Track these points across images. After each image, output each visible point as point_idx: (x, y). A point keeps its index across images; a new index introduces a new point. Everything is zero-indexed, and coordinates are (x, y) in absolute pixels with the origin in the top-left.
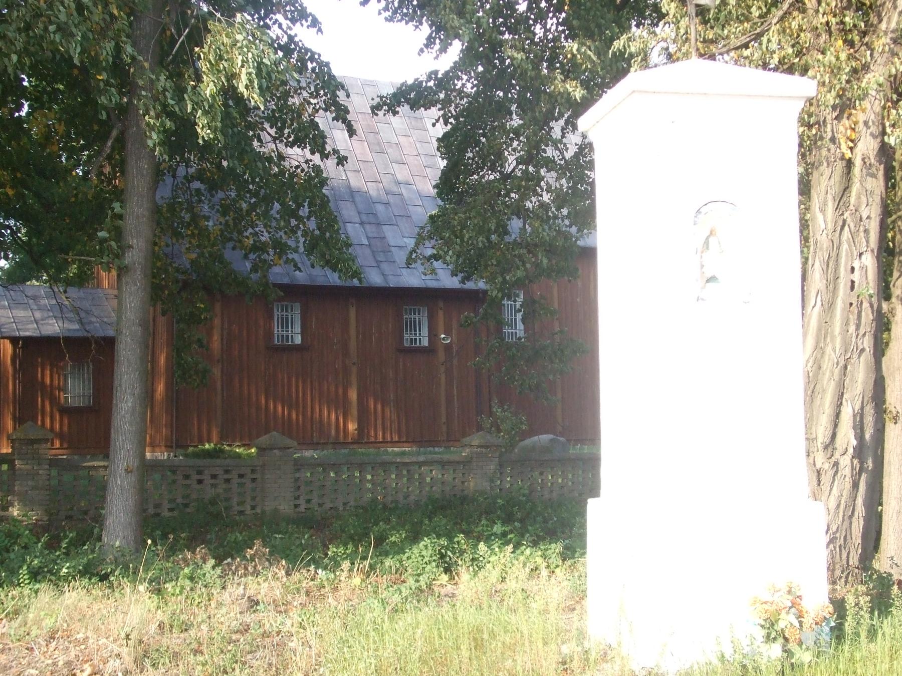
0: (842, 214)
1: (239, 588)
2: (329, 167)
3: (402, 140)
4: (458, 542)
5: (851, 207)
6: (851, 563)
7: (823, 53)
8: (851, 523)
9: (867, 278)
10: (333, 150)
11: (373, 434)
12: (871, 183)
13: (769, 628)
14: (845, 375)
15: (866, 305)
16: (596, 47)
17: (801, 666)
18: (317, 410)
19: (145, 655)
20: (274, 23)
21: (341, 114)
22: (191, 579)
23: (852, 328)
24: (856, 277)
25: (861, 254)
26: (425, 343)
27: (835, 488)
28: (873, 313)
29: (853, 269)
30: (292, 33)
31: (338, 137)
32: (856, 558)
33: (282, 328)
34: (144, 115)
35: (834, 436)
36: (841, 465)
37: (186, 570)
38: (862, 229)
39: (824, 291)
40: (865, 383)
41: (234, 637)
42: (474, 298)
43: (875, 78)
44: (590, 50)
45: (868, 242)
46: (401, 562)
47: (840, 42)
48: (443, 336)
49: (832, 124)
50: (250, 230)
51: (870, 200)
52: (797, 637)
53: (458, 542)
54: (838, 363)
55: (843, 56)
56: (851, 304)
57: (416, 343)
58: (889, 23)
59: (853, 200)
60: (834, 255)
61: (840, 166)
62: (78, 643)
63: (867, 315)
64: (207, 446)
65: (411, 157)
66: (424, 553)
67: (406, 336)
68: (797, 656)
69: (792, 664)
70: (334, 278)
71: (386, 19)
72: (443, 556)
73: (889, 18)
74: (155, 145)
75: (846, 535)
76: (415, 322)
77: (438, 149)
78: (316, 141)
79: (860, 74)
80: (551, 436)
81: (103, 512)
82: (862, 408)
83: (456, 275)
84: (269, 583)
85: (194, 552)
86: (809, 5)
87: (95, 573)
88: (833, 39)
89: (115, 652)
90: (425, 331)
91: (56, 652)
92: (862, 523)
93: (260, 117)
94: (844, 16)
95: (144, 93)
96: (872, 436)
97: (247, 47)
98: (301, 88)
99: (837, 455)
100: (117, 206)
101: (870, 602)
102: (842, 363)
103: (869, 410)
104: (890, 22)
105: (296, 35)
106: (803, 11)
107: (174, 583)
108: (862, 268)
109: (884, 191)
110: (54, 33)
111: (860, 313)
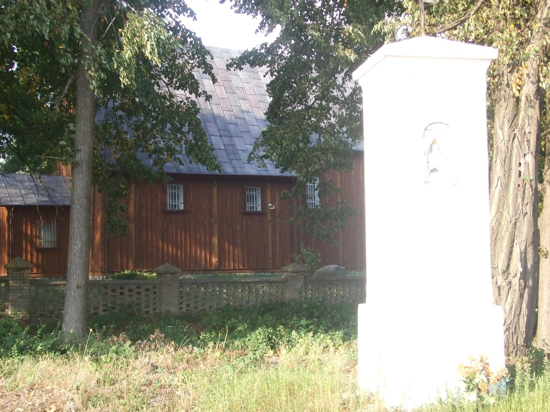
0: (514, 131)
1: (146, 358)
2: (201, 102)
3: (245, 85)
4: (279, 331)
5: (519, 126)
6: (519, 343)
7: (502, 32)
8: (519, 319)
9: (528, 169)
10: (203, 91)
11: (227, 264)
12: (531, 112)
13: (469, 383)
14: (515, 228)
15: (528, 186)
16: (363, 29)
17: (488, 406)
18: (193, 250)
19: (89, 399)
20: (167, 14)
21: (208, 70)
22: (117, 353)
23: (520, 200)
24: (522, 169)
25: (525, 155)
26: (259, 209)
27: (509, 298)
28: (532, 191)
29: (520, 164)
30: (178, 20)
31: (206, 84)
32: (522, 340)
33: (172, 200)
34: (88, 70)
35: (508, 266)
36: (513, 284)
37: (114, 348)
38: (525, 139)
39: (503, 177)
40: (528, 233)
41: (143, 388)
42: (289, 182)
43: (533, 47)
44: (360, 31)
45: (529, 147)
46: (244, 342)
47: (512, 26)
48: (270, 205)
49: (507, 76)
50: (153, 140)
51: (531, 122)
52: (486, 388)
53: (279, 331)
54: (511, 221)
55: (514, 34)
56: (519, 185)
57: (253, 209)
58: (542, 14)
59: (520, 122)
60: (508, 155)
61: (512, 101)
62: (48, 392)
63: (529, 192)
64: (126, 272)
65: (251, 96)
66: (259, 337)
67: (247, 205)
68: (486, 400)
69: (483, 405)
70: (203, 170)
71: (235, 12)
72: (270, 339)
73: (542, 11)
74: (94, 88)
75: (516, 326)
76: (253, 196)
77: (267, 91)
78: (193, 86)
79: (525, 45)
80: (336, 266)
81: (63, 312)
82: (526, 249)
83: (278, 168)
84: (164, 355)
85: (118, 337)
86: (493, 3)
87: (58, 349)
88: (508, 24)
89: (70, 397)
90: (259, 202)
91: (34, 397)
92: (526, 319)
93: (159, 72)
94: (515, 10)
95: (88, 57)
96: (532, 266)
97: (150, 28)
98: (183, 54)
99: (510, 277)
100: (71, 125)
101: (530, 367)
102: (513, 221)
103: (530, 250)
104: (543, 14)
105: (180, 21)
106: (490, 7)
107: (106, 355)
108: (525, 163)
109: (539, 117)
110: (33, 20)
111: (524, 191)
